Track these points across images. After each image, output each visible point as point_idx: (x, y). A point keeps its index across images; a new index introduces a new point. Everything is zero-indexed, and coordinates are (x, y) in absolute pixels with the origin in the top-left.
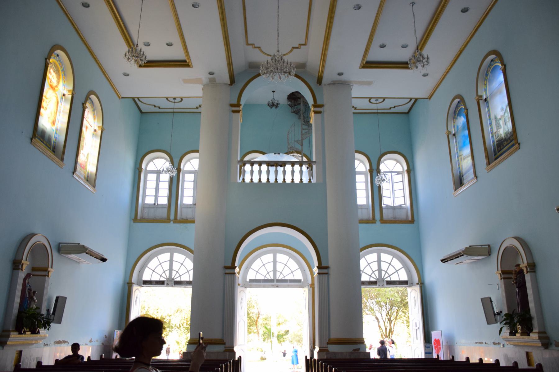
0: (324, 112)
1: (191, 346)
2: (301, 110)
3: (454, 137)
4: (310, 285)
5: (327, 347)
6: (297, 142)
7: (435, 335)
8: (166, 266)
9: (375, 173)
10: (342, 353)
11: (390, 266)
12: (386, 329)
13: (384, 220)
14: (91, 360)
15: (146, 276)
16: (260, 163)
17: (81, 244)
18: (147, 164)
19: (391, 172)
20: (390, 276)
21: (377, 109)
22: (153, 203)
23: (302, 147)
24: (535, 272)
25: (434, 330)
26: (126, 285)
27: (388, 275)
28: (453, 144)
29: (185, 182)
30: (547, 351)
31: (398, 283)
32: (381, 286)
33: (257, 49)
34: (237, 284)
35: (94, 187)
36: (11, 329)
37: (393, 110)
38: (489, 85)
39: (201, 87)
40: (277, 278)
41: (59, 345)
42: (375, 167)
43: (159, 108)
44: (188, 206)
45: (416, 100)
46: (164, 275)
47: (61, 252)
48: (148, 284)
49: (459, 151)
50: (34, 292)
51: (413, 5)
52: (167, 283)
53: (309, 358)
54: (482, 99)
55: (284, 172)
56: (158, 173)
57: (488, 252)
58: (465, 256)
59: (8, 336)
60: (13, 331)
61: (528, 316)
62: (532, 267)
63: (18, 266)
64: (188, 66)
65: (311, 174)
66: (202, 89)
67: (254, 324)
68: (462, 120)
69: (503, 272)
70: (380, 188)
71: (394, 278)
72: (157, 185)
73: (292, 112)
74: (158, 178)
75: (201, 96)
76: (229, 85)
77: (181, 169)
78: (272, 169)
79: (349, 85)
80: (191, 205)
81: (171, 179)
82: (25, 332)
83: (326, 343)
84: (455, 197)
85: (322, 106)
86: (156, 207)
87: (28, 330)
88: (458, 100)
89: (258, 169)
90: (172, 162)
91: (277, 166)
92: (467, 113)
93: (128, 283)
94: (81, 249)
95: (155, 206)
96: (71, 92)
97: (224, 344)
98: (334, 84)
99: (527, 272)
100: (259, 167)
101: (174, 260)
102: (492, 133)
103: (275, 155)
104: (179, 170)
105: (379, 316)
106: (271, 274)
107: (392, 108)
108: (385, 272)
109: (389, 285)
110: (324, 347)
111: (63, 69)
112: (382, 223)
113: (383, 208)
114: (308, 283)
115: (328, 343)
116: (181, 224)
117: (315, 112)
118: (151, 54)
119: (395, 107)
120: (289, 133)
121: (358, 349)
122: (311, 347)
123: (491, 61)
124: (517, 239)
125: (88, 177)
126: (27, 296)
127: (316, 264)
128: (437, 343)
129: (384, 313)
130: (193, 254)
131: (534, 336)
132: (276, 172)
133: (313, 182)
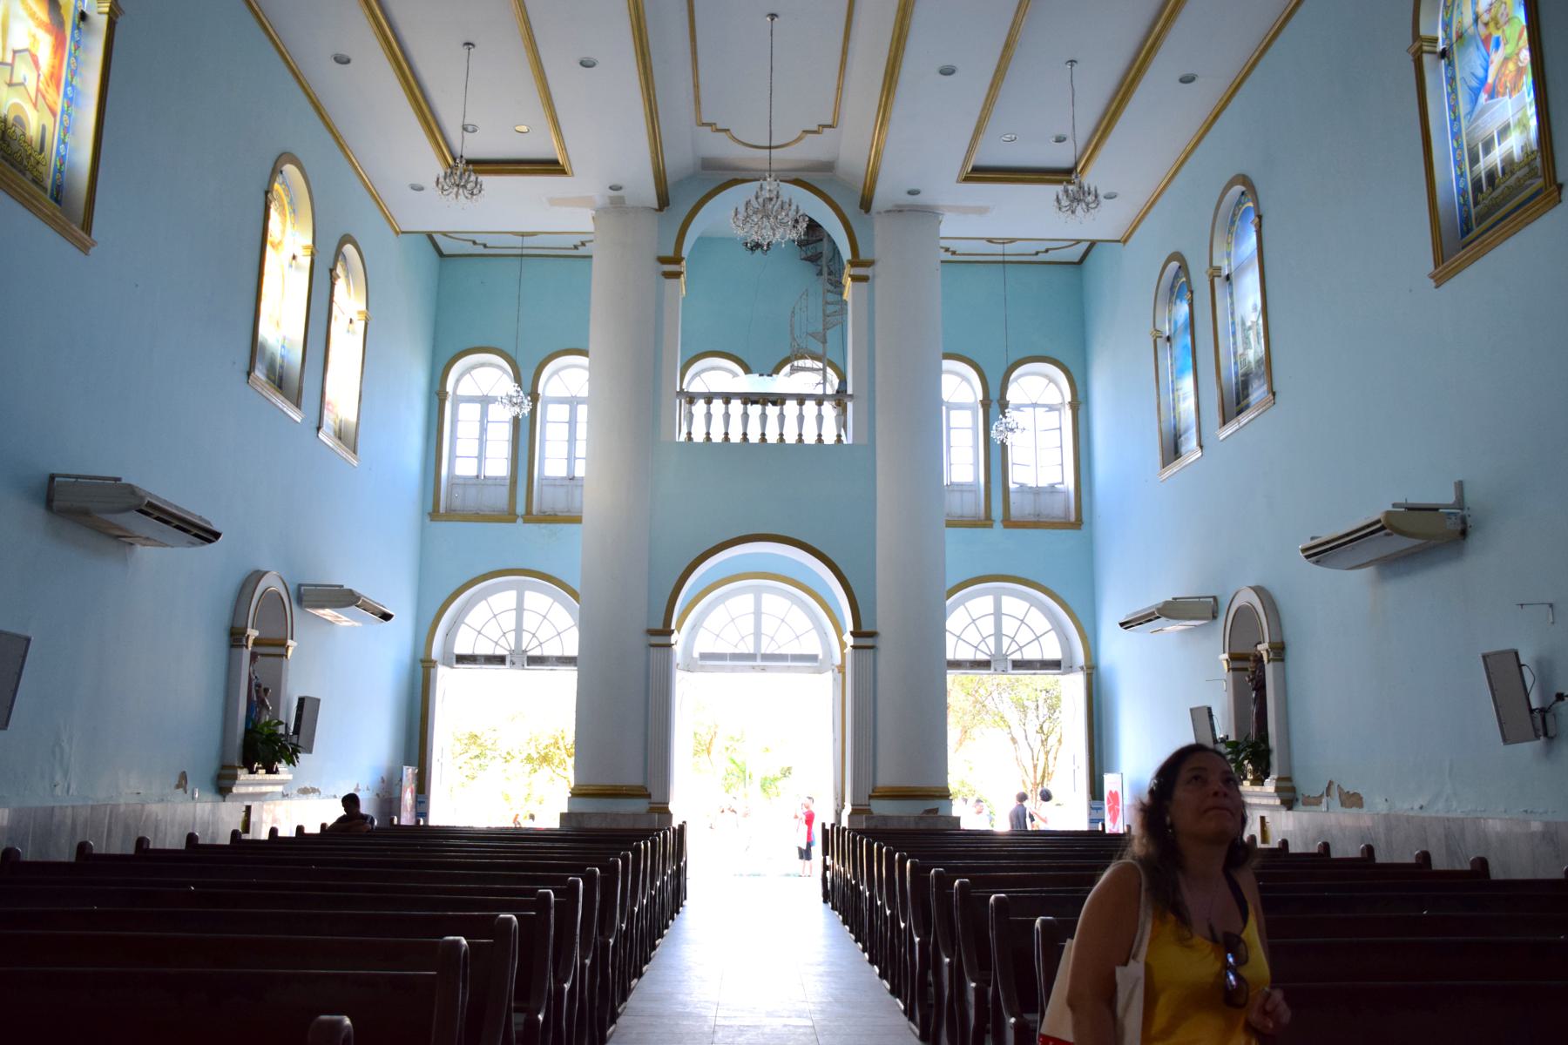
0: (874, 276)
1: (577, 800)
2: (824, 256)
3: (1168, 344)
4: (837, 667)
5: (869, 805)
6: (813, 335)
7: (1110, 782)
8: (509, 621)
9: (995, 408)
10: (900, 818)
11: (1023, 625)
12: (1035, 766)
13: (1012, 519)
14: (148, 850)
15: (461, 648)
16: (727, 398)
17: (346, 587)
18: (458, 381)
19: (1034, 405)
20: (1020, 648)
21: (1004, 255)
22: (474, 473)
23: (824, 348)
24: (1283, 660)
25: (1110, 771)
26: (420, 666)
27: (1017, 647)
28: (1166, 362)
29: (548, 425)
30: (1290, 812)
31: (1038, 665)
32: (999, 671)
33: (722, 134)
34: (674, 665)
35: (355, 452)
36: (237, 765)
37: (1041, 257)
38: (1236, 245)
39: (590, 213)
40: (763, 652)
41: (305, 796)
42: (995, 395)
43: (485, 246)
44: (554, 482)
45: (1093, 244)
46: (503, 642)
47: (304, 603)
48: (468, 664)
49: (1177, 378)
50: (266, 690)
51: (1072, 66)
52: (511, 661)
53: (828, 827)
54: (1219, 276)
55: (782, 417)
56: (485, 401)
57: (1211, 611)
58: (1163, 619)
59: (235, 777)
60: (241, 768)
61: (1263, 746)
62: (1279, 651)
63: (241, 640)
64: (563, 172)
65: (842, 423)
66: (593, 218)
67: (703, 750)
68: (1183, 309)
69: (1234, 657)
70: (1004, 447)
71: (1031, 654)
72: (483, 430)
73: (802, 259)
74: (484, 414)
75: (592, 230)
76: (656, 210)
77: (539, 395)
78: (755, 410)
79: (934, 213)
80: (562, 478)
81: (516, 421)
82: (257, 768)
83: (867, 798)
84: (1162, 482)
85: (869, 264)
86: (483, 485)
87: (260, 766)
88: (1239, 188)
89: (723, 411)
90: (518, 379)
91: (764, 404)
92: (1192, 300)
93: (422, 661)
94: (345, 598)
95: (479, 481)
96: (310, 250)
97: (649, 796)
98: (900, 211)
99: (1269, 661)
100: (724, 406)
101: (525, 607)
102: (1235, 353)
103: (761, 378)
104: (534, 397)
105: (1019, 734)
106: (750, 640)
107: (1042, 252)
108: (1010, 640)
109: (1018, 669)
110: (861, 805)
111: (291, 200)
112: (1006, 526)
113: (1011, 490)
114: (833, 665)
115: (871, 797)
116: (543, 525)
117: (855, 279)
118: (475, 147)
119: (1047, 251)
120: (793, 312)
121: (936, 811)
122: (838, 805)
123: (1240, 194)
124: (1259, 590)
125: (340, 430)
126: (255, 699)
127: (849, 626)
128: (1113, 799)
129: (1033, 726)
130: (578, 603)
131: (1270, 786)
132: (764, 417)
133: (845, 442)
